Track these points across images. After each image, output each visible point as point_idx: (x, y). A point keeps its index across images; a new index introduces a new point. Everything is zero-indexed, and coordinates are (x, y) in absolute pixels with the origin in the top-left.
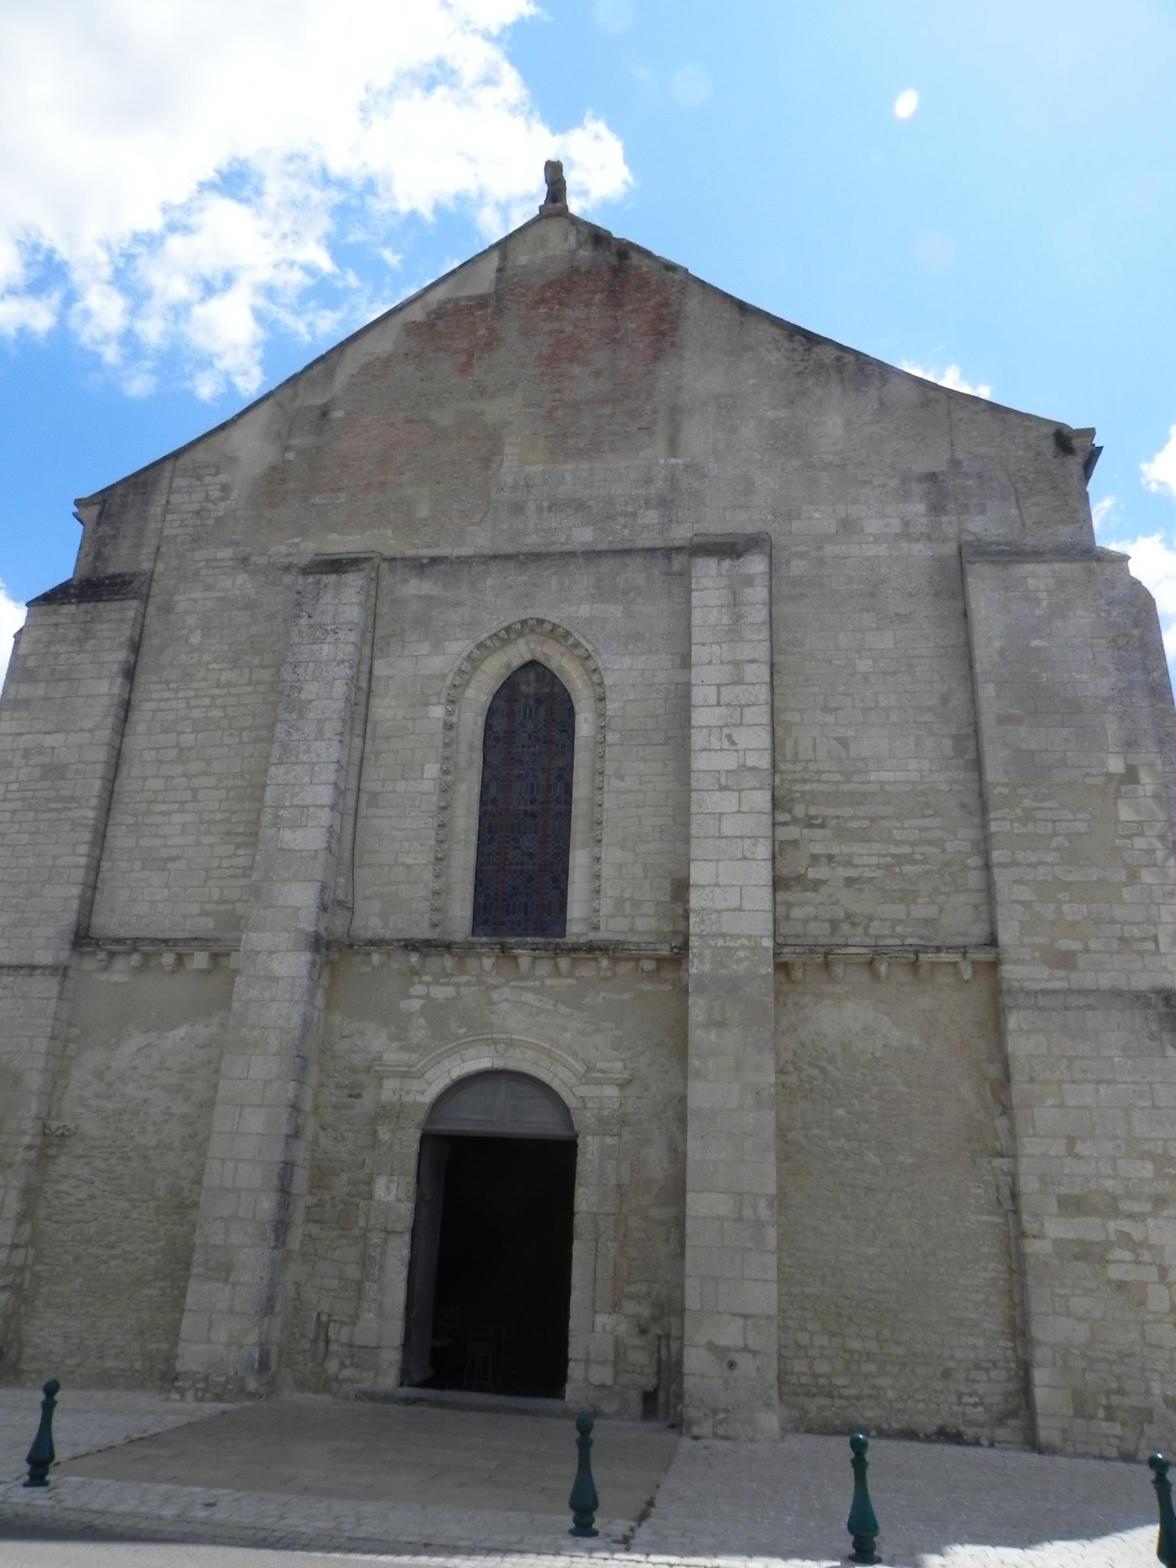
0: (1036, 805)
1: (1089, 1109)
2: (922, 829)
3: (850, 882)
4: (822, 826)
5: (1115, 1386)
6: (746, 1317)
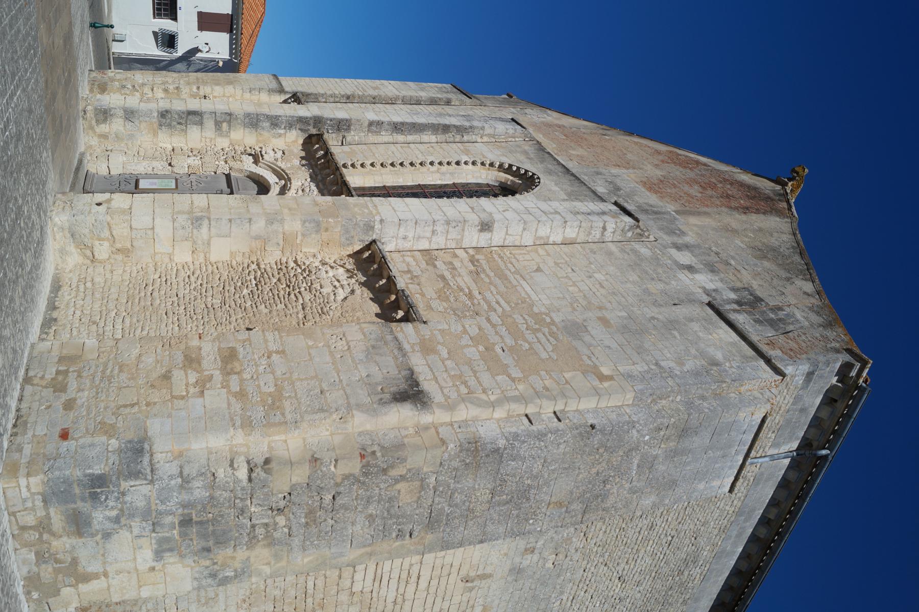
0: (547, 334)
1: (311, 359)
2: (498, 303)
3: (443, 277)
4: (474, 266)
5: (84, 374)
6: (130, 208)
